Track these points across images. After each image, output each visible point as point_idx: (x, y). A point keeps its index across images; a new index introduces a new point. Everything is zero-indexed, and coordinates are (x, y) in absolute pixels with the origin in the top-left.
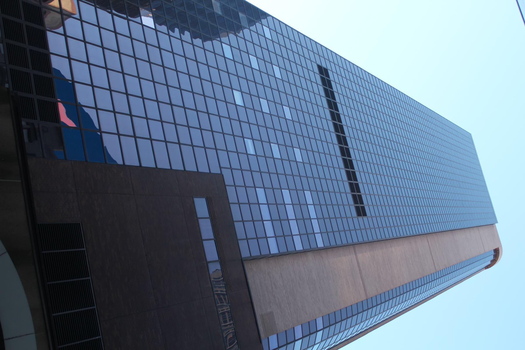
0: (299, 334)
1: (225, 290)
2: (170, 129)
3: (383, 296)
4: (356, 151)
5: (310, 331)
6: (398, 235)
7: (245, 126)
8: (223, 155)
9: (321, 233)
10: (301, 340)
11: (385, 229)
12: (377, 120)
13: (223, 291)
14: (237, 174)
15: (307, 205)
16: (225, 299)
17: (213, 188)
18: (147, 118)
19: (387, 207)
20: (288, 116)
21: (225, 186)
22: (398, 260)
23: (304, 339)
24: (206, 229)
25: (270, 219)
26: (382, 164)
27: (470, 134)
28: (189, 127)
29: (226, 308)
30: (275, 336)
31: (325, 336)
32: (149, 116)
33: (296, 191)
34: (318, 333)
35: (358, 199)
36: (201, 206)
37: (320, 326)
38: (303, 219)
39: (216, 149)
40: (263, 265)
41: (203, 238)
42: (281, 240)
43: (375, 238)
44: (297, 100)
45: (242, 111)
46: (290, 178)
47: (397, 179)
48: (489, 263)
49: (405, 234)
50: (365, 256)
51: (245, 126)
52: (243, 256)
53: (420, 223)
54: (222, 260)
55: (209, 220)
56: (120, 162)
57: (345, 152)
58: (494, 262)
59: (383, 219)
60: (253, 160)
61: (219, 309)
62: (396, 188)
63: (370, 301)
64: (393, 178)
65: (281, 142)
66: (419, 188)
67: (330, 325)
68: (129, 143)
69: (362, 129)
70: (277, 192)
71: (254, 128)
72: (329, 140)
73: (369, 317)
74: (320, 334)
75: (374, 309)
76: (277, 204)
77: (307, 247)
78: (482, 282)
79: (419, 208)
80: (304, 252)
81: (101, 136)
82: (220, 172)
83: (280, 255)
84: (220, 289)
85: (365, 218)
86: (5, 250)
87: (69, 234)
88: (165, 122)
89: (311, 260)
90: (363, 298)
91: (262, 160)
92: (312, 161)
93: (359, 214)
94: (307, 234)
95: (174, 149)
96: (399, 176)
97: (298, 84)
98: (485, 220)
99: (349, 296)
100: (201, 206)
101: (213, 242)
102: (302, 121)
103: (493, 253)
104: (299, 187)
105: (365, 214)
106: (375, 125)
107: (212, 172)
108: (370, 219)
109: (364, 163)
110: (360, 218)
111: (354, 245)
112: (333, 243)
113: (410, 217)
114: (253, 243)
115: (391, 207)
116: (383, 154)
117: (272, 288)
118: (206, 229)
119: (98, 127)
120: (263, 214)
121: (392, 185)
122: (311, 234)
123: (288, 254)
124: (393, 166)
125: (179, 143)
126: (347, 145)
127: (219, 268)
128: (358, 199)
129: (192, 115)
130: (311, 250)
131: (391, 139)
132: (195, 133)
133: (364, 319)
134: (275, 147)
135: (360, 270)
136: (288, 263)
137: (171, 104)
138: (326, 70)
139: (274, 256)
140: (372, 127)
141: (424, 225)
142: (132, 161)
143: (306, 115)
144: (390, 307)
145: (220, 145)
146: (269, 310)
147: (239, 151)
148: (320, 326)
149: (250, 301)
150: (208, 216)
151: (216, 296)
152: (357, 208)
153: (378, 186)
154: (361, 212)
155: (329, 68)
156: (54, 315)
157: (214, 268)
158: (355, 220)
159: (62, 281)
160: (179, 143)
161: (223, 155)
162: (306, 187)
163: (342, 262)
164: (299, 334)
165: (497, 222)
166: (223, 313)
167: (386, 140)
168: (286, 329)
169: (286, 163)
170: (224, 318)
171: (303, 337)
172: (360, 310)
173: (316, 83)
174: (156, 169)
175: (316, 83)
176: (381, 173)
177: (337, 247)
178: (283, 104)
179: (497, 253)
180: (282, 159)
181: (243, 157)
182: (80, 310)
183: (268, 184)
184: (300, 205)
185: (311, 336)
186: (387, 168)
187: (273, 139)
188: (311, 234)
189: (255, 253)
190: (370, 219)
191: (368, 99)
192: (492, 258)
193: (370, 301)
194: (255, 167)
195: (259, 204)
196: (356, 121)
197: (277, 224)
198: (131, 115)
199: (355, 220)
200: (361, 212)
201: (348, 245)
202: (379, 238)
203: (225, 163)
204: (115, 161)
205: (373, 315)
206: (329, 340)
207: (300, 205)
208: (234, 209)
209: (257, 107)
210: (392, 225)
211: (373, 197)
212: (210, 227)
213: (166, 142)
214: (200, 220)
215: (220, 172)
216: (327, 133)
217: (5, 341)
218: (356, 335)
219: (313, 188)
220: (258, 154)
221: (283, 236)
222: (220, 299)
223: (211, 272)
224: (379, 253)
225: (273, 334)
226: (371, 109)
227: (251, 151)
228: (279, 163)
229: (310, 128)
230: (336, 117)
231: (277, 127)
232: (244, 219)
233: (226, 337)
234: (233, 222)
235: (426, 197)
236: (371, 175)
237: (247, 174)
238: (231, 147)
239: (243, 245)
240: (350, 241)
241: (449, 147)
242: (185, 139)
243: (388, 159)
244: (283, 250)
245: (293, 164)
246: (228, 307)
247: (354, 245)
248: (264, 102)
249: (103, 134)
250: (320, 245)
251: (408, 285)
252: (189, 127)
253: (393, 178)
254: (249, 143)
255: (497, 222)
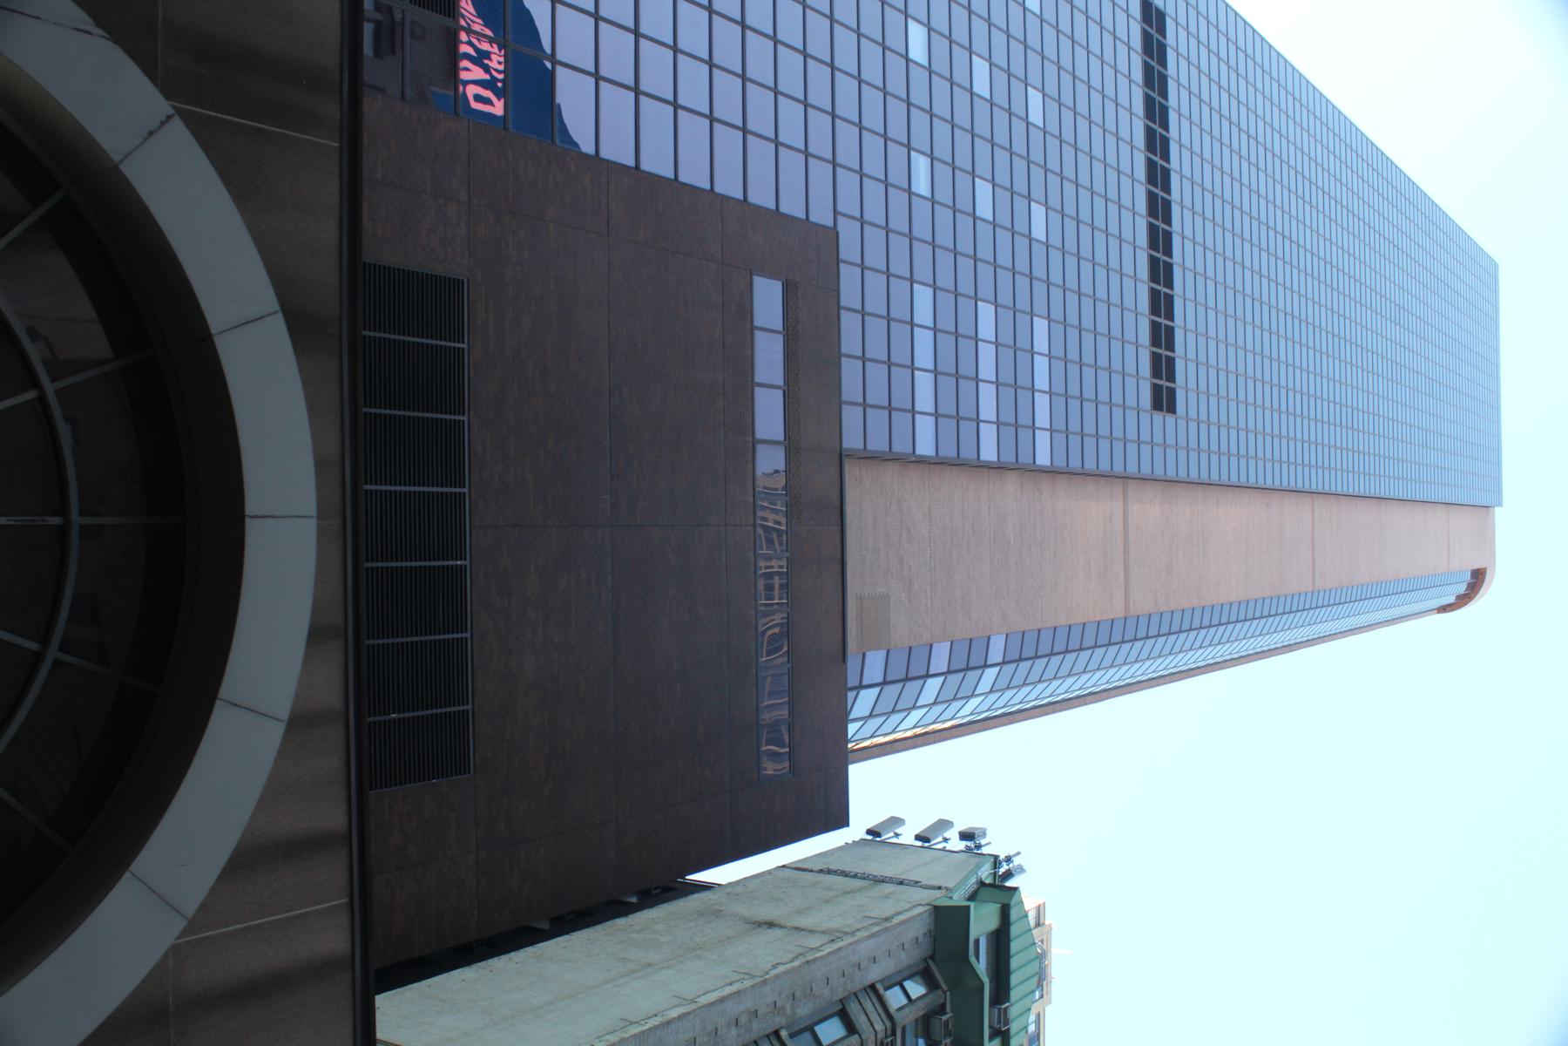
0: (940, 662)
1: (783, 520)
2: (728, 87)
3: (1187, 615)
4: (1189, 245)
5: (968, 662)
6: (1277, 483)
7: (920, 120)
8: (848, 181)
9: (1051, 430)
10: (877, 689)
11: (1234, 460)
12: (1262, 175)
13: (779, 523)
14: (875, 237)
15: (976, 340)
16: (780, 542)
17: (807, 259)
18: (675, 49)
19: (1251, 409)
20: (981, 87)
21: (838, 260)
22: (1229, 539)
23: (950, 677)
24: (769, 358)
25: (932, 367)
26: (1210, 273)
27: (1496, 265)
28: (806, 105)
29: (778, 565)
30: (882, 654)
31: (1001, 684)
32: (716, 60)
33: (1015, 313)
34: (988, 671)
35: (1163, 367)
36: (767, 299)
37: (996, 655)
38: (1015, 386)
39: (834, 164)
40: (889, 475)
41: (757, 380)
42: (948, 426)
43: (1204, 476)
44: (1067, 79)
45: (919, 78)
46: (945, 259)
47: (1240, 325)
48: (1451, 599)
49: (1261, 481)
50: (1148, 510)
51: (920, 120)
52: (846, 445)
53: (1260, 454)
54: (792, 444)
55: (780, 338)
56: (587, 147)
57: (1160, 240)
58: (1464, 599)
59: (1233, 433)
60: (922, 210)
61: (762, 563)
62: (1267, 361)
63: (1131, 623)
64: (1282, 341)
65: (1003, 178)
66: (1283, 358)
67: (1021, 659)
68: (618, 103)
69: (1218, 191)
70: (1023, 320)
71: (1002, 157)
72: (1127, 201)
73: (1120, 660)
74: (991, 674)
75: (1138, 644)
76: (958, 335)
77: (1008, 457)
78: (1418, 644)
79: (1284, 417)
80: (999, 467)
81: (552, 74)
82: (831, 224)
83: (937, 462)
84: (773, 517)
85: (1170, 419)
86: (277, 307)
87: (432, 301)
88: (646, 37)
89: (1010, 492)
90: (1118, 612)
91: (944, 216)
92: (1071, 246)
93: (1157, 405)
94: (1016, 426)
95: (729, 141)
96: (1282, 332)
97: (1080, 36)
98: (1465, 490)
99: (1086, 600)
100: (767, 299)
101: (780, 393)
102: (1068, 135)
103: (1468, 577)
104: (966, 287)
105: (1172, 409)
106: (1217, 162)
107: (812, 218)
108: (1182, 423)
109: (1200, 280)
110: (1158, 416)
111: (1126, 478)
112: (1075, 463)
113: (1284, 442)
114: (878, 419)
115: (1242, 407)
116: (1273, 276)
117: (900, 538)
118: (769, 358)
119: (548, 50)
120: (909, 352)
121: (1222, 336)
122: (970, 419)
123: (957, 464)
124: (1239, 287)
125: (744, 130)
126: (1169, 223)
127: (782, 466)
128: (1163, 367)
129: (791, 62)
130: (955, 464)
131: (1271, 224)
132: (791, 113)
133: (1120, 660)
134: (921, 165)
135: (1126, 543)
136: (954, 491)
137: (743, 25)
138: (1161, 16)
139: (923, 461)
140: (1207, 167)
141: (1269, 465)
142: (617, 150)
143: (1083, 124)
144: (1176, 649)
145: (847, 155)
146: (880, 590)
147: (865, 170)
148: (996, 655)
149: (839, 555)
150: (779, 326)
151: (760, 530)
152: (1156, 390)
153: (1258, 359)
154: (1164, 400)
155: (1170, 10)
156: (368, 487)
157: (770, 461)
158: (1145, 418)
159: (398, 488)
160: (637, 90)
161: (848, 181)
162: (1040, 307)
163: (1090, 514)
164: (940, 662)
165: (1500, 505)
166: (770, 576)
167: (1287, 242)
168: (913, 643)
169: (1004, 237)
170: (769, 588)
171: (949, 672)
172: (1103, 639)
173: (1128, 45)
174: (674, 185)
175: (1128, 45)
176: (1201, 298)
177: (1083, 474)
178: (974, 48)
179: (1478, 579)
180: (994, 224)
181: (898, 199)
182: (407, 488)
183: (943, 151)
184: (1014, 348)
185: (970, 674)
186: (1257, 304)
187: (983, 167)
188: (970, 419)
189: (878, 443)
190: (1182, 423)
191: (1194, 72)
192: (1462, 589)
193: (1131, 623)
194: (922, 229)
195: (912, 324)
196: (1246, 191)
197: (948, 384)
198: (636, 33)
199: (1145, 418)
200: (1164, 400)
201: (1109, 476)
202: (1215, 477)
203: (848, 204)
204: (576, 145)
205: (1132, 658)
206: (1009, 694)
207: (1014, 348)
208: (849, 323)
209: (961, 76)
210: (1252, 453)
211: (1241, 380)
212: (779, 357)
213: (712, 119)
214: (758, 334)
215: (831, 224)
216: (1126, 182)
217: (248, 520)
218: (1078, 697)
219: (1054, 201)
220: (937, 198)
221: (957, 417)
222: (770, 541)
223: (759, 473)
224: (1186, 511)
225: (878, 648)
226: (1252, 143)
227: (922, 185)
228: (984, 231)
229: (1084, 160)
230: (1157, 144)
231: (1001, 137)
232: (868, 355)
233: (764, 633)
234: (840, 355)
235: (1298, 387)
236: (1211, 314)
237: (899, 245)
238: (874, 166)
239: (851, 417)
240: (1119, 468)
241: (1427, 281)
242: (760, 121)
243: (1281, 289)
244: (948, 451)
245: (1022, 243)
246: (784, 563)
247: (1126, 478)
248: (1035, 97)
249: (559, 69)
250: (1043, 459)
251: (1235, 608)
252: (806, 105)
253: (1231, 322)
254: (984, 189)
255: (1500, 505)
